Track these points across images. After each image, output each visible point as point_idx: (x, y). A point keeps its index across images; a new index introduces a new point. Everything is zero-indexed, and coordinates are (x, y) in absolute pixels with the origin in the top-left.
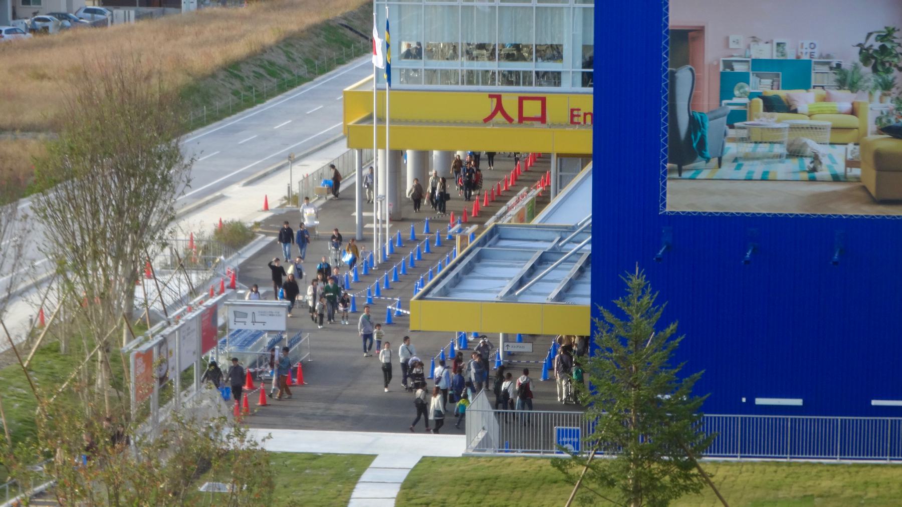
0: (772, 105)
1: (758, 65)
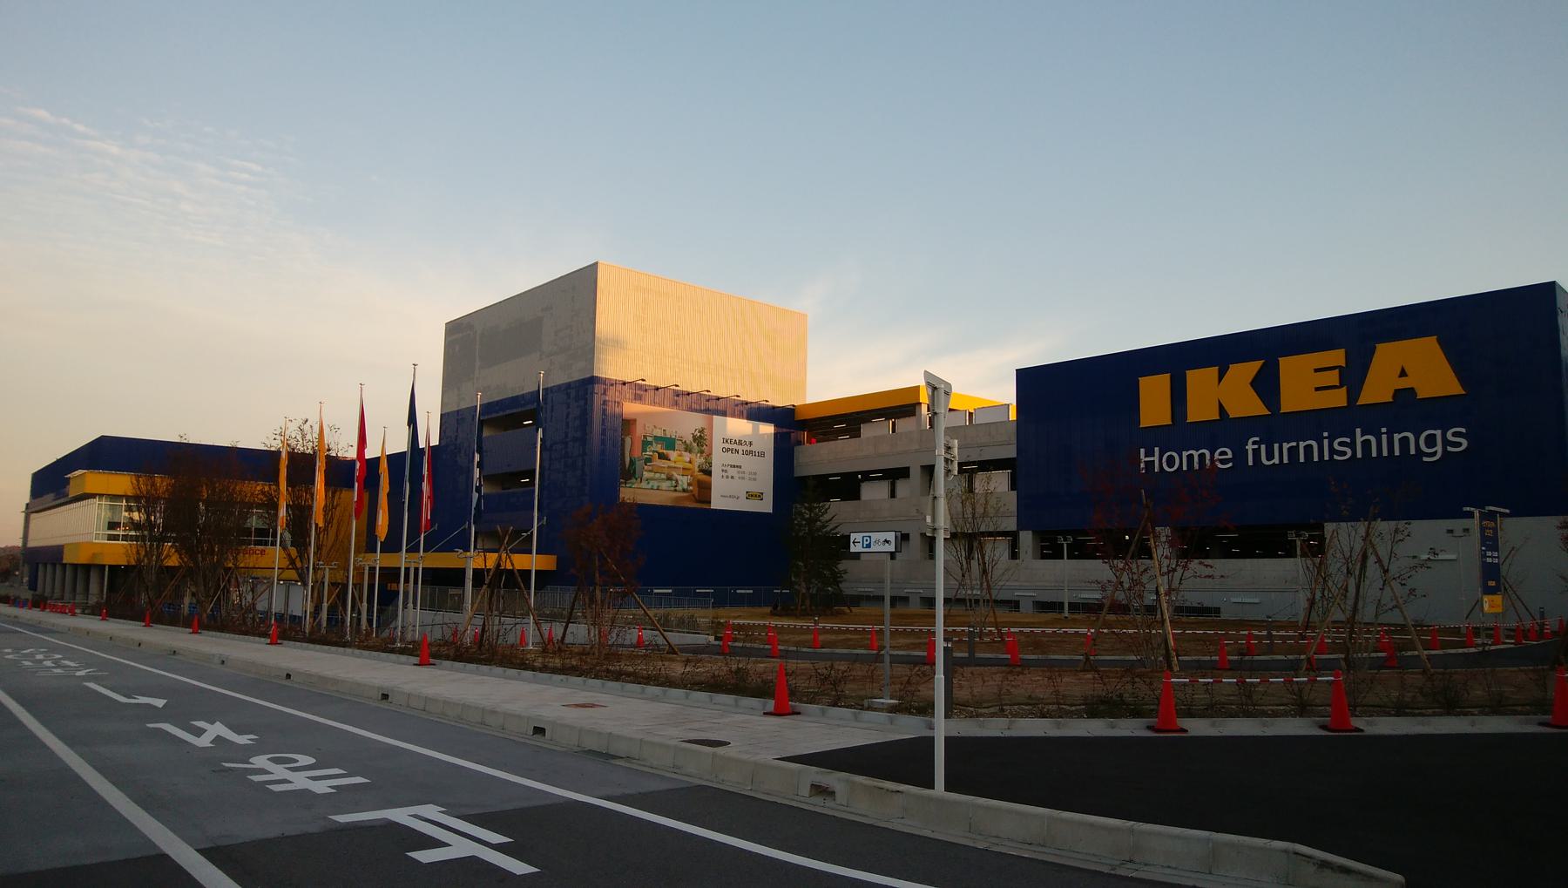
0: (662, 457)
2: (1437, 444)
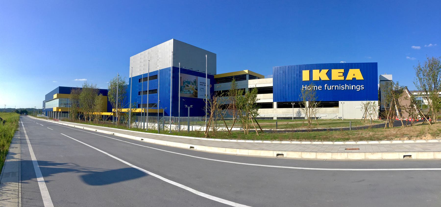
0: (187, 86)
1: (186, 81)
2: (360, 88)
